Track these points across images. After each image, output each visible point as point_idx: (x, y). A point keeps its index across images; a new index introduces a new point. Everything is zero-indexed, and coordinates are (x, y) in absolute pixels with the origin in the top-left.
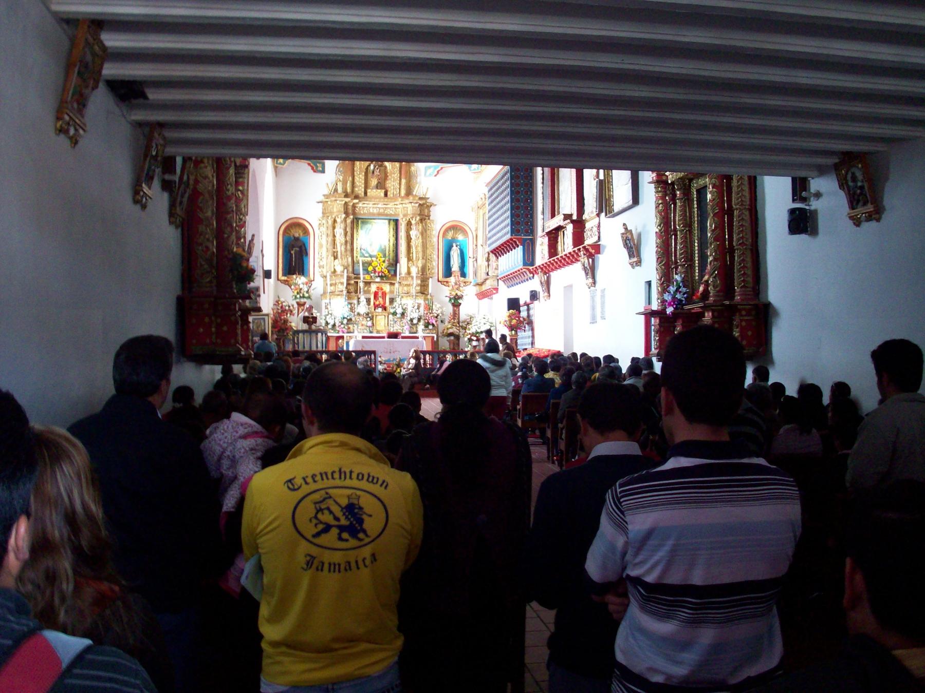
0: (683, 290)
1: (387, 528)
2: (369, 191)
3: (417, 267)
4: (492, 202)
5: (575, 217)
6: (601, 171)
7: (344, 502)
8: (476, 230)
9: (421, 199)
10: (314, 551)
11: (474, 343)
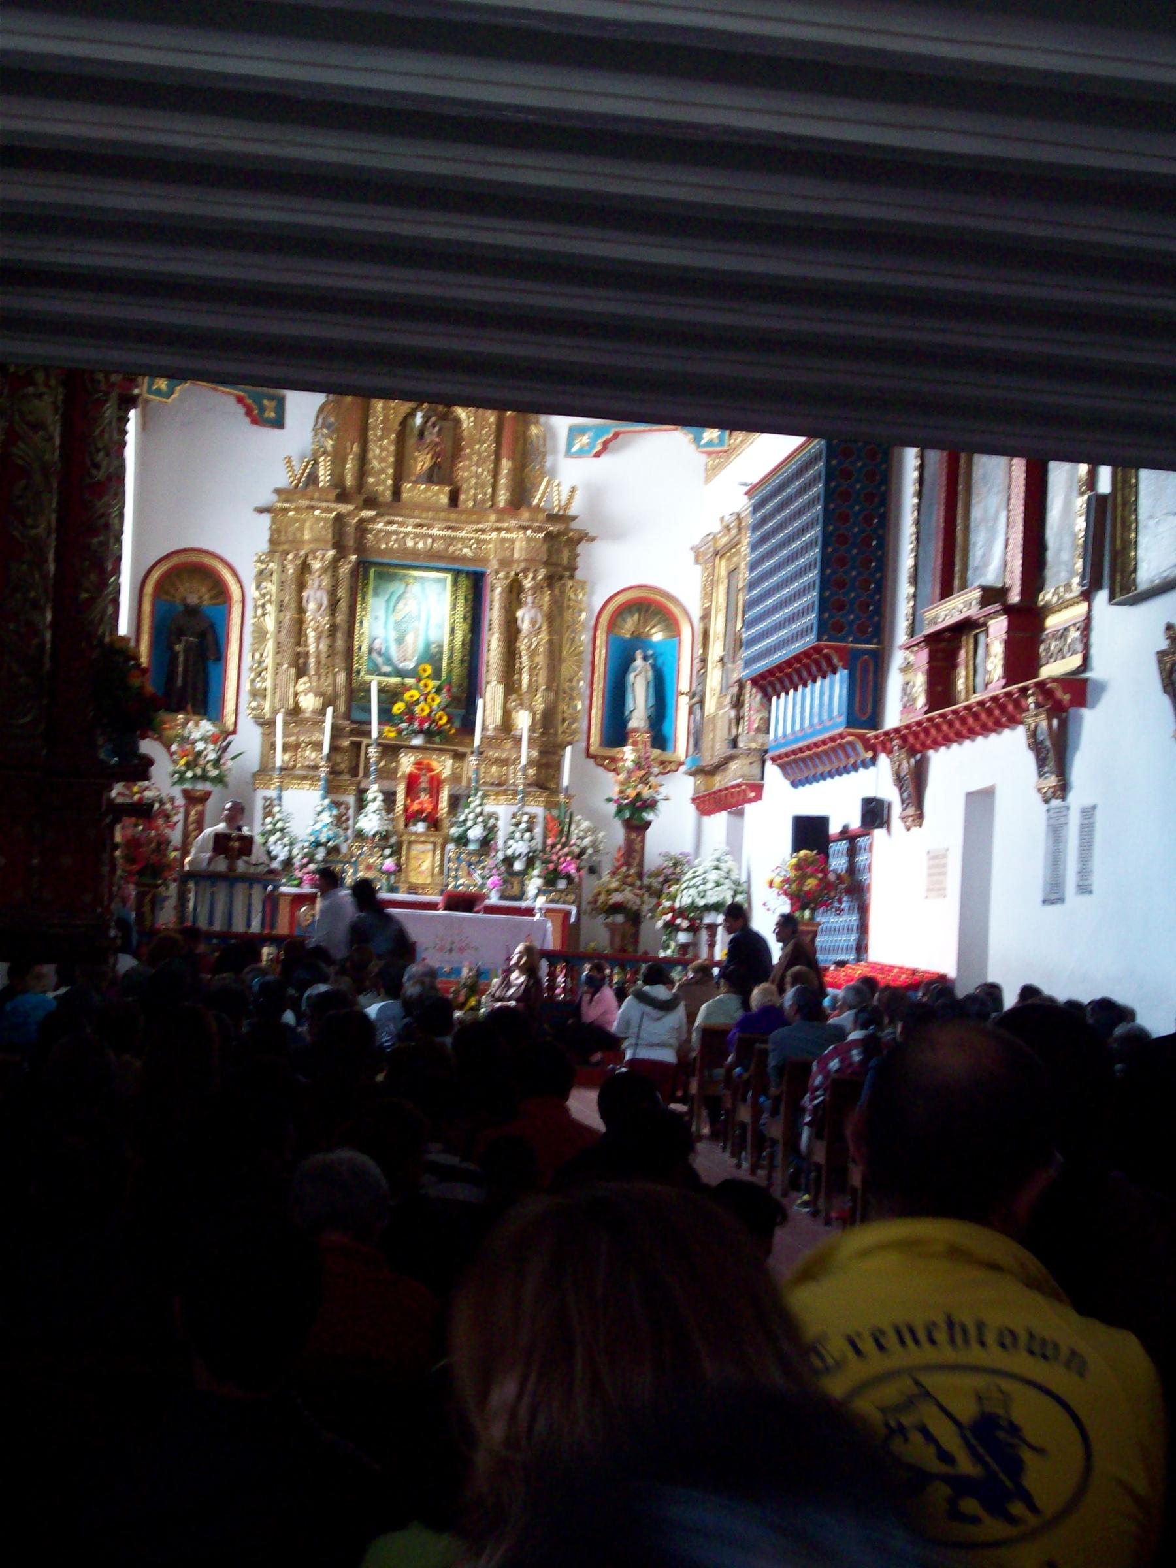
3: (531, 710)
4: (764, 539)
5: (1014, 598)
6: (1105, 474)
7: (966, 1410)
8: (706, 616)
9: (552, 518)
11: (682, 937)
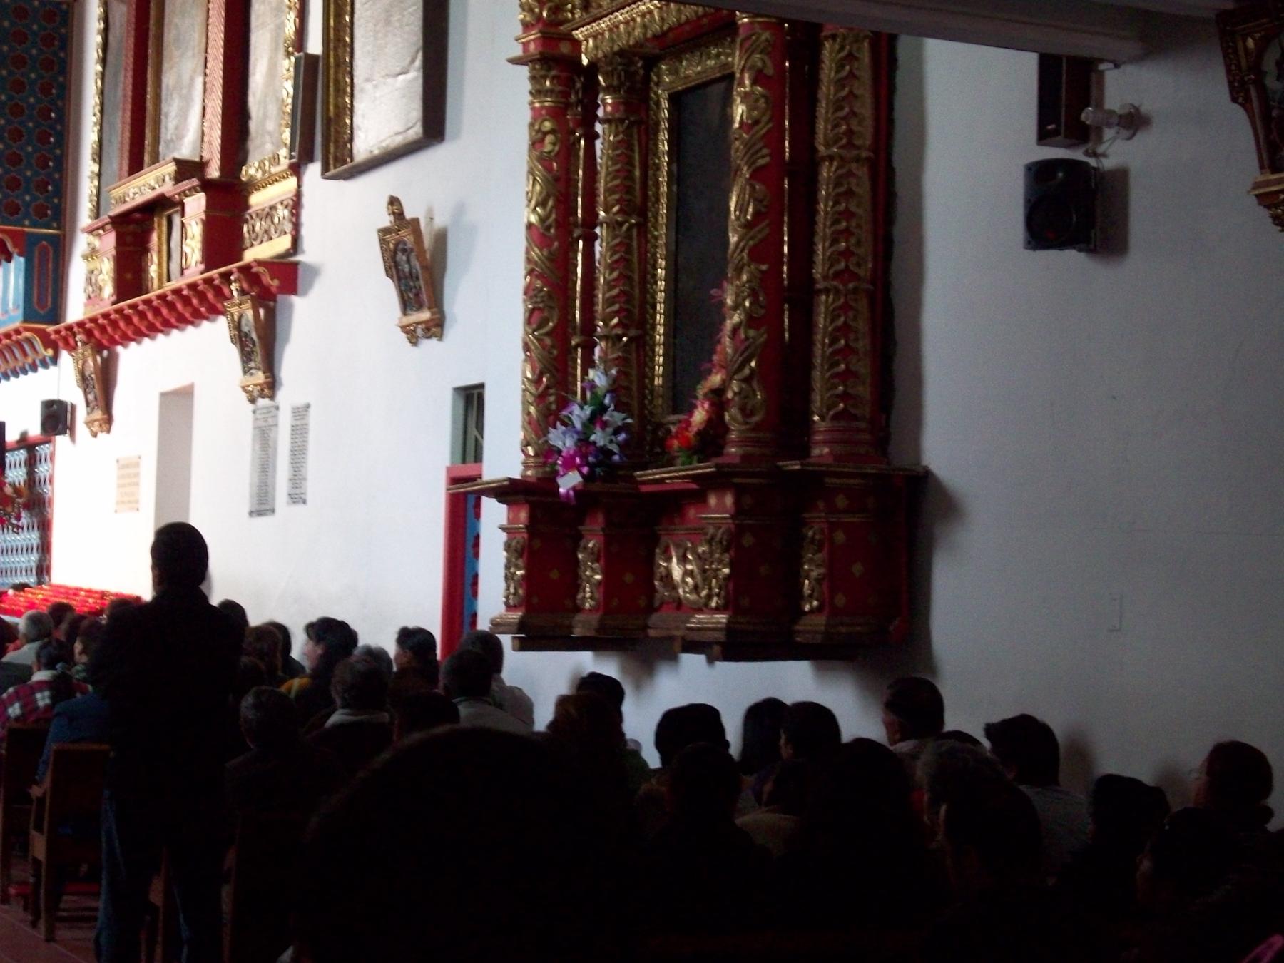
0: (614, 417)
5: (214, 172)
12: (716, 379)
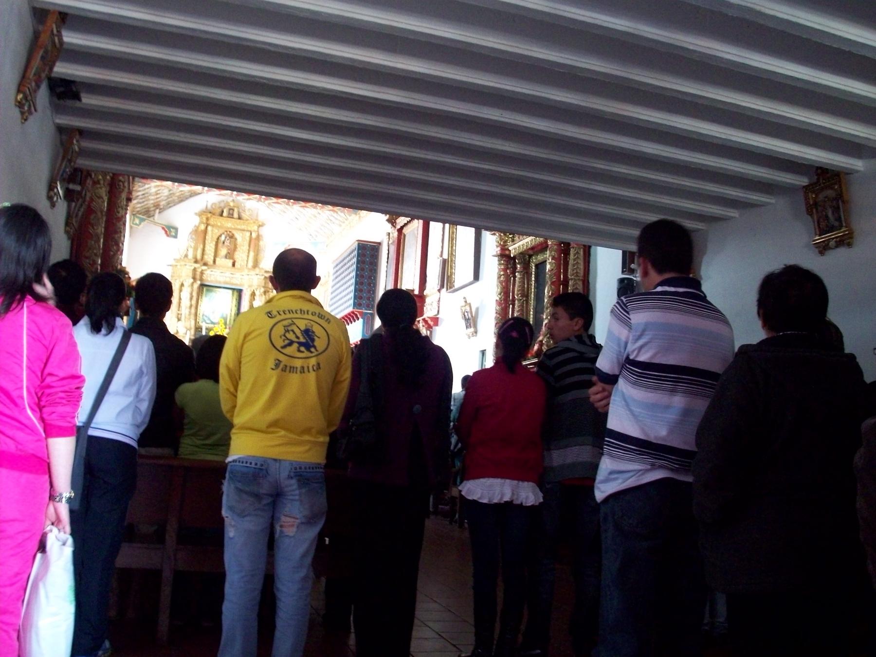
1: (329, 349)
2: (217, 259)
7: (303, 328)
10: (282, 357)
12: (541, 338)
